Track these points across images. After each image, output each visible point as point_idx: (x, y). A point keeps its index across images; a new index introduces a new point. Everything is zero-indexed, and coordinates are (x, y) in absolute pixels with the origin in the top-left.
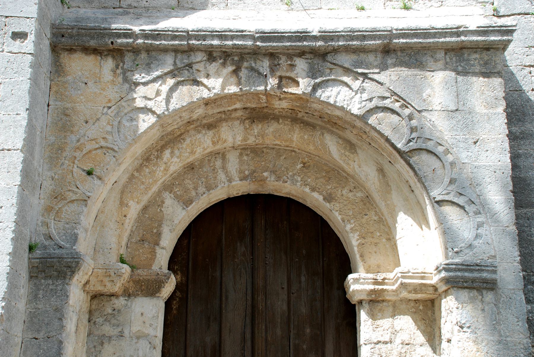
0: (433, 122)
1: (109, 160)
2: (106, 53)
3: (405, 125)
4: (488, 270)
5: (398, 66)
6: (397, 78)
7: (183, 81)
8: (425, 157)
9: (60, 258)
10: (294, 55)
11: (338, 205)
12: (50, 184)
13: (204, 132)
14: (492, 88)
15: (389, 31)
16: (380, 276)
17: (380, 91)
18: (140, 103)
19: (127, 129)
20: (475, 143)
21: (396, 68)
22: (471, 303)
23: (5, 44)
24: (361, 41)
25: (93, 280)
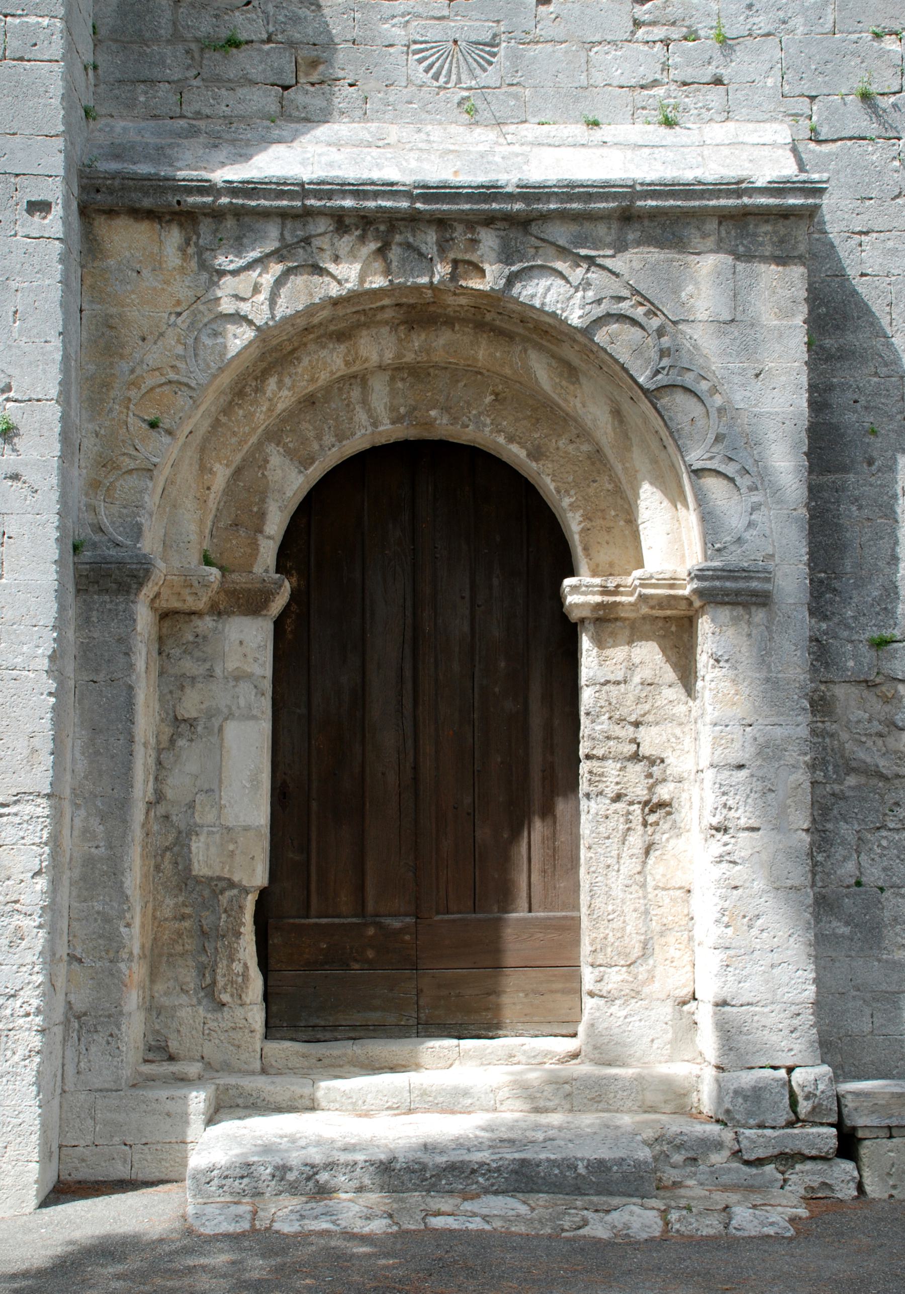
1: (182, 403)
2: (168, 218)
3: (651, 344)
4: (759, 578)
5: (643, 245)
6: (641, 266)
7: (296, 267)
8: (680, 398)
9: (121, 563)
10: (478, 223)
11: (550, 466)
12: (93, 443)
13: (331, 346)
15: (630, 187)
18: (227, 306)
19: (209, 351)
20: (757, 376)
21: (641, 249)
22: (732, 625)
23: (18, 223)
24: (585, 202)
25: (165, 592)
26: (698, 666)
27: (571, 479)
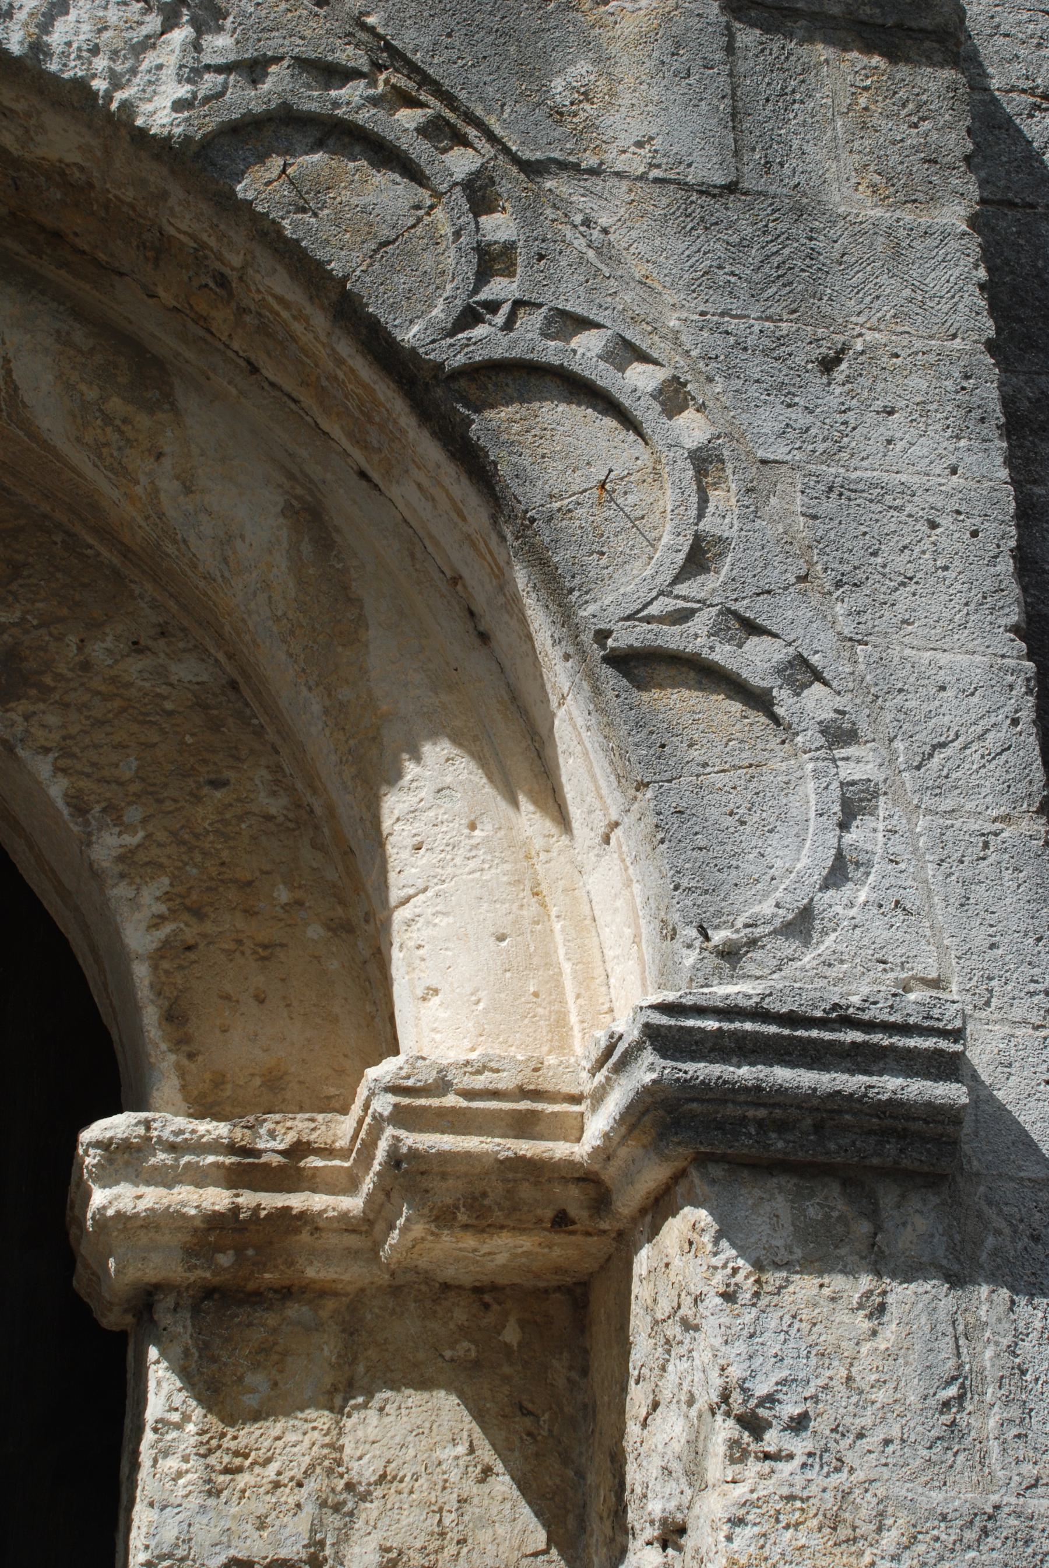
0: (605, 231)
3: (447, 230)
11: (52, 720)
14: (911, 106)
16: (272, 1135)
17: (308, 33)
20: (828, 365)
26: (633, 1474)
27: (128, 768)
